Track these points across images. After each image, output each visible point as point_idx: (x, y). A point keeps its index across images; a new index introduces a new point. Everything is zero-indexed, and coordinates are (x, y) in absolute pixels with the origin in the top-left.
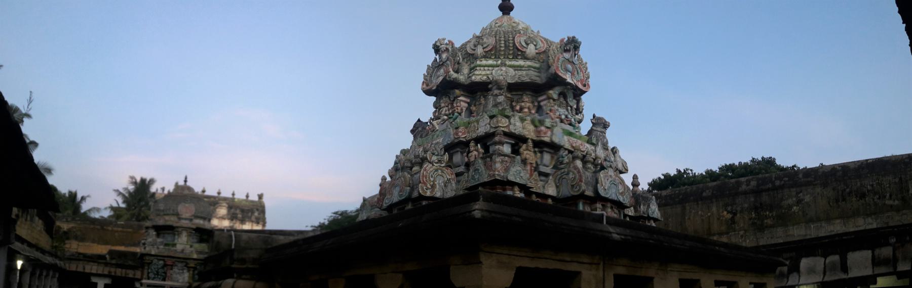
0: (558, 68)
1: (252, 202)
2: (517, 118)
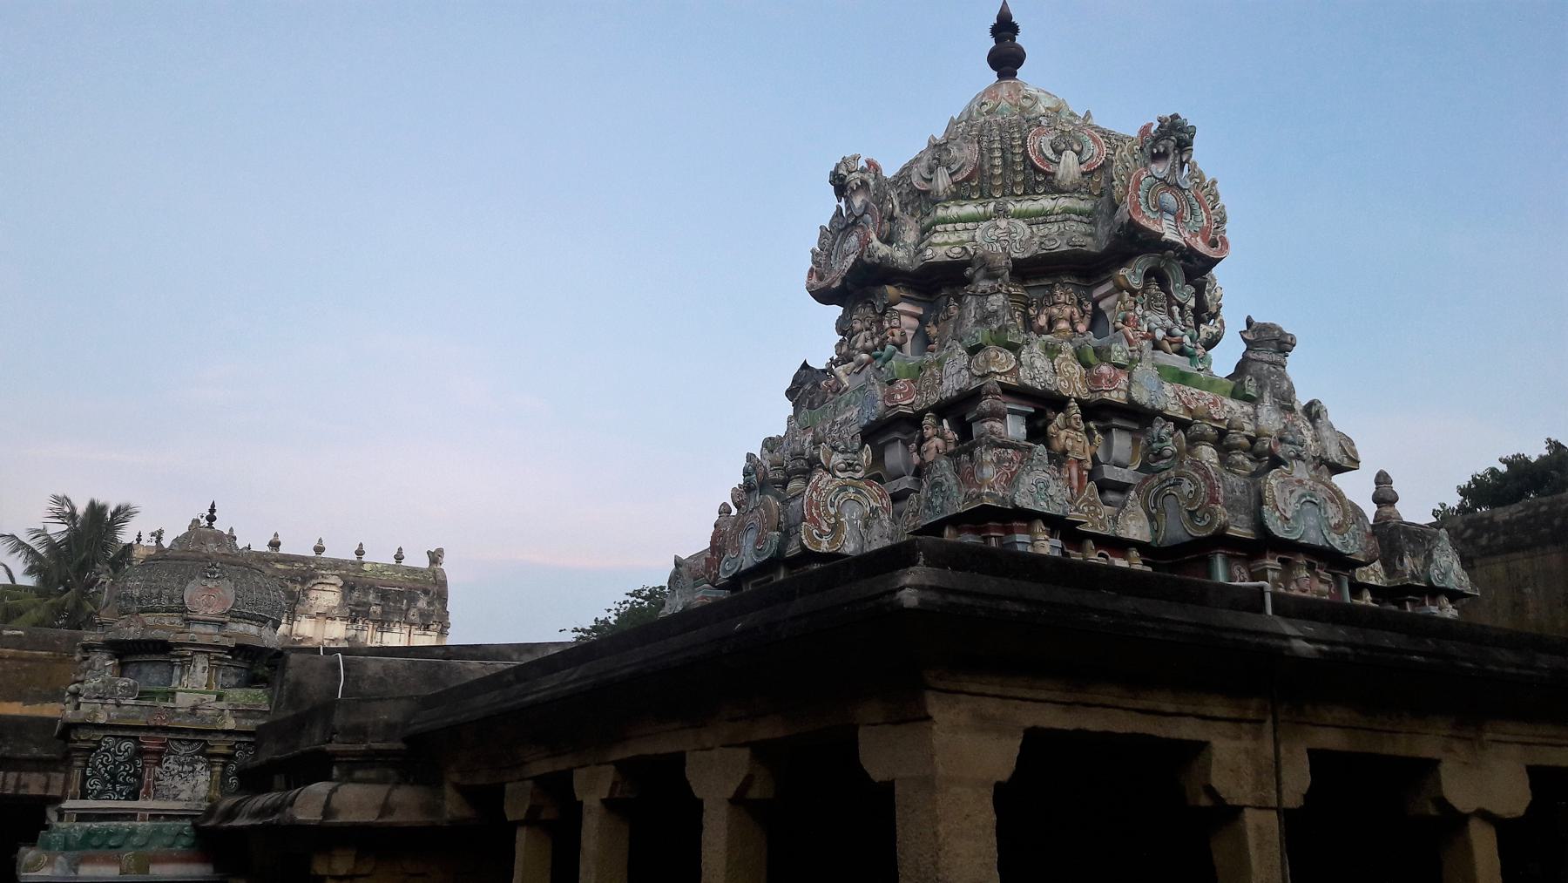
0: (1137, 206)
1: (413, 570)
2: (1036, 348)
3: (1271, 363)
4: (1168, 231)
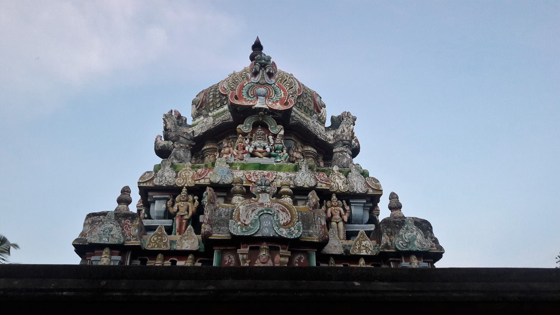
3: (340, 152)
4: (259, 104)
